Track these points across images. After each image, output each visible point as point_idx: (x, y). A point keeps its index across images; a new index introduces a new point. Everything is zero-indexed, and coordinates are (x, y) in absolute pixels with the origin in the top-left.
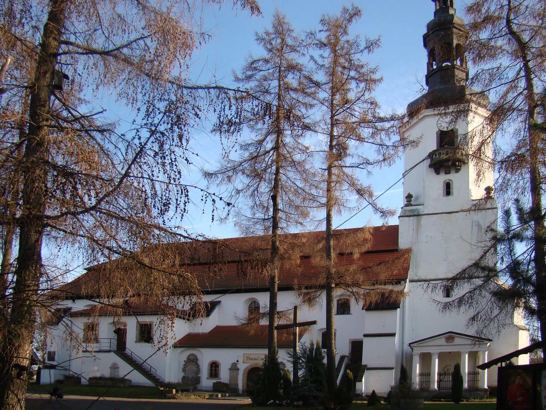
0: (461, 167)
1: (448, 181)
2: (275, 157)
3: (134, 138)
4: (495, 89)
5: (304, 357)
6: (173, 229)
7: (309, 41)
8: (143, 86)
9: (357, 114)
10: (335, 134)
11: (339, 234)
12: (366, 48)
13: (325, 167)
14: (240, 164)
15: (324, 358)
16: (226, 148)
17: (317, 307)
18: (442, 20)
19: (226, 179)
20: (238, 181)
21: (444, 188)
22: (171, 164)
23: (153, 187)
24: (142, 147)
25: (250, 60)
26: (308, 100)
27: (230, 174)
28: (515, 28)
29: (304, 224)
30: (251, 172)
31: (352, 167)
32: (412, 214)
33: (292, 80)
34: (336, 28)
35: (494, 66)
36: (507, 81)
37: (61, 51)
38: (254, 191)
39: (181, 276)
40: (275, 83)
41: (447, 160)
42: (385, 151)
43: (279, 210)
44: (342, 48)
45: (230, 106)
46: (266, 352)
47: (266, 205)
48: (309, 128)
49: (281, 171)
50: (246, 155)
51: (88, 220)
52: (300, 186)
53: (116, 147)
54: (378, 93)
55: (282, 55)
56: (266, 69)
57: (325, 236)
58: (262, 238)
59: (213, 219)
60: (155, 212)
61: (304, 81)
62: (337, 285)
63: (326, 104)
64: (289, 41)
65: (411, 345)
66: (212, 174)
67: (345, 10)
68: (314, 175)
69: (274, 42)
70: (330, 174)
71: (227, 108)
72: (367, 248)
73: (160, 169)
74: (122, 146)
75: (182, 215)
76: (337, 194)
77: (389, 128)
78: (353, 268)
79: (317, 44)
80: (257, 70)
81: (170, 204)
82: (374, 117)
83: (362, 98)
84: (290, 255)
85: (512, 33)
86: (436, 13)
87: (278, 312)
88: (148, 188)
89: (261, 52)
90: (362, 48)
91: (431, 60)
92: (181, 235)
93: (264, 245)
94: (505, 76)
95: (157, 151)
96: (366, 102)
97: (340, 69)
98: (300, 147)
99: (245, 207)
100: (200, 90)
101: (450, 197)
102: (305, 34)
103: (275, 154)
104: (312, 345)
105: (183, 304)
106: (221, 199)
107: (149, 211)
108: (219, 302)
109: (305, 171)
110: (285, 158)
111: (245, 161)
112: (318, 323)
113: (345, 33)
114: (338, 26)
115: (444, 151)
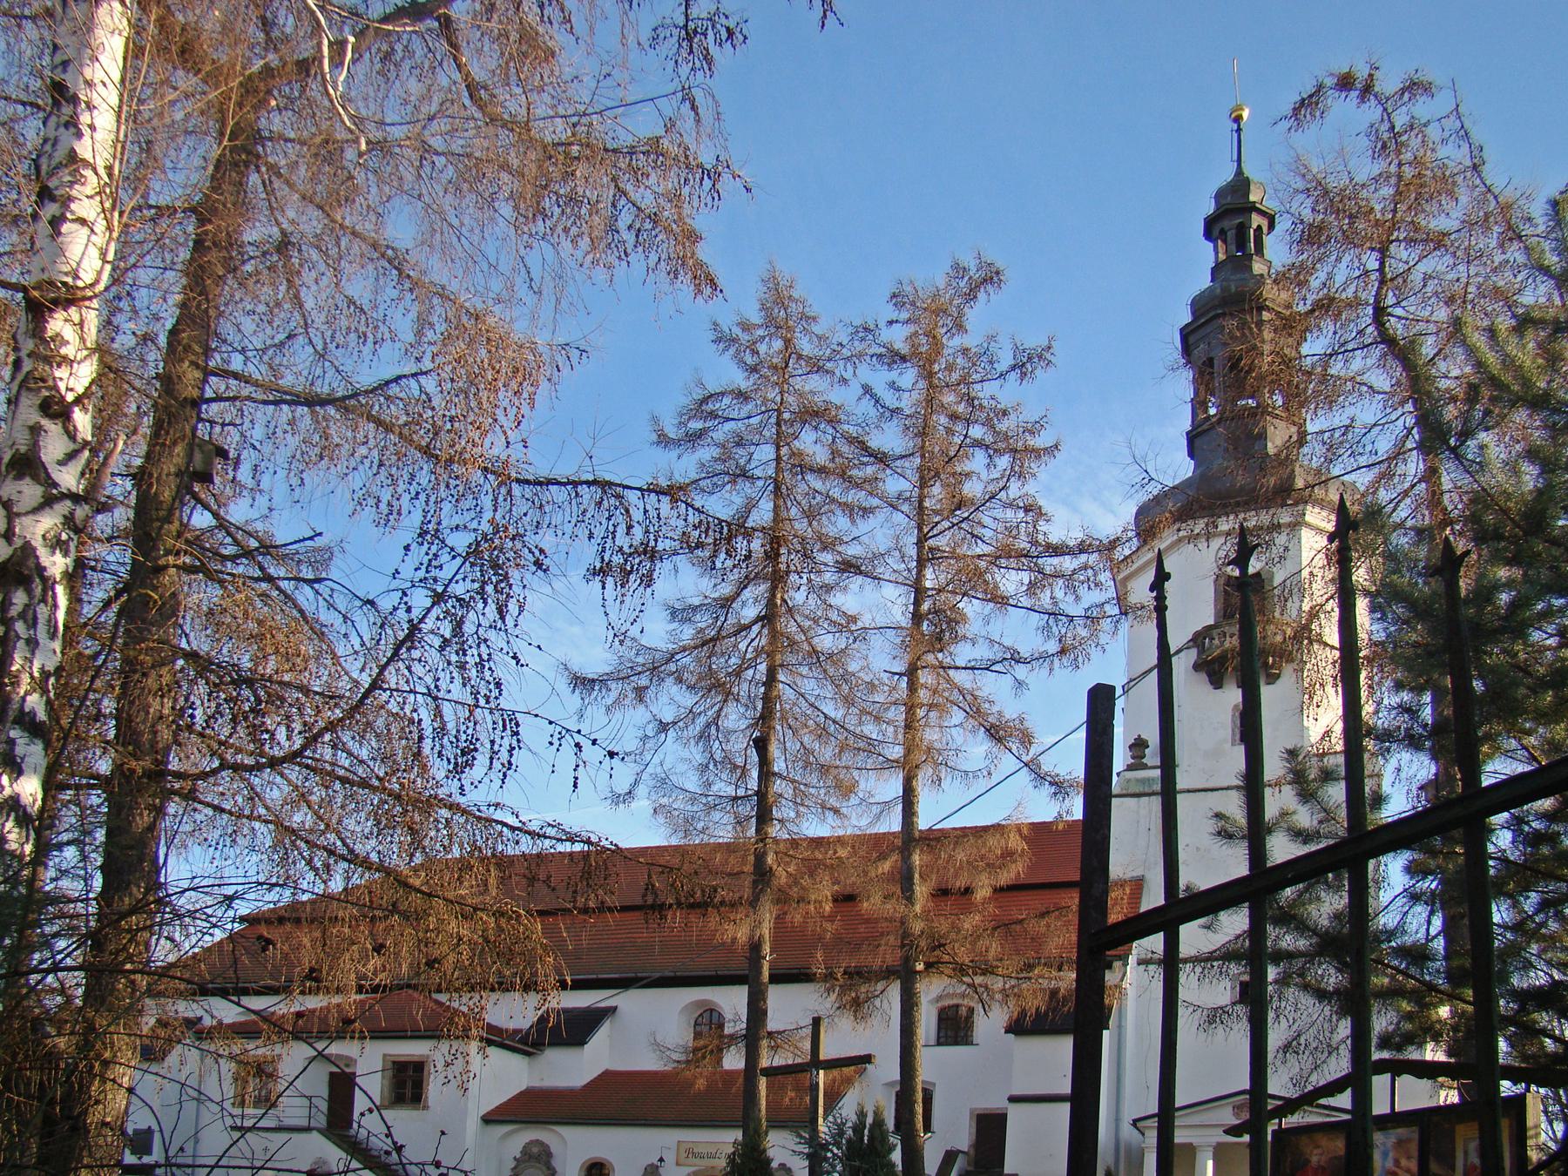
2: (764, 641)
3: (395, 609)
5: (838, 1144)
6: (484, 808)
7: (859, 346)
8: (413, 477)
9: (988, 533)
10: (928, 584)
11: (934, 838)
12: (1013, 368)
13: (900, 667)
14: (671, 657)
15: (892, 1148)
16: (616, 624)
17: (875, 1021)
18: (1233, 289)
19: (631, 695)
20: (664, 699)
22: (480, 665)
23: (438, 713)
24: (414, 628)
25: (698, 394)
26: (855, 496)
27: (644, 681)
28: (1396, 327)
29: (844, 810)
30: (700, 679)
31: (973, 668)
32: (1147, 790)
33: (812, 444)
34: (935, 315)
35: (1337, 422)
36: (1374, 459)
37: (209, 393)
38: (708, 726)
39: (502, 914)
40: (767, 452)
43: (775, 774)
44: (950, 368)
45: (630, 527)
46: (738, 1135)
47: (740, 761)
48: (858, 568)
49: (781, 677)
50: (687, 634)
51: (275, 789)
52: (832, 715)
53: (345, 617)
54: (1041, 484)
55: (785, 381)
56: (743, 415)
57: (898, 842)
58: (729, 848)
59: (575, 786)
60: (439, 769)
61: (845, 448)
62: (929, 965)
63: (905, 508)
64: (805, 346)
65: (1139, 1124)
66: (593, 681)
67: (959, 270)
68: (872, 687)
69: (762, 348)
70: (912, 687)
71: (621, 530)
72: (1013, 875)
73: (455, 674)
74: (364, 622)
75: (505, 775)
76: (931, 735)
77: (1074, 572)
78: (970, 922)
79: (880, 356)
80: (716, 417)
81: (476, 750)
82: (1035, 543)
84: (803, 888)
85: (1387, 340)
86: (1215, 271)
87: (770, 1034)
88: (425, 715)
89: (727, 373)
90: (1003, 366)
92: (505, 824)
93: (733, 863)
94: (1369, 448)
95: (448, 636)
96: (1011, 505)
97: (943, 420)
98: (834, 616)
99: (682, 767)
100: (553, 488)
102: (850, 330)
103: (765, 631)
104: (862, 1115)
105: (515, 1011)
106: (594, 742)
107: (424, 768)
108: (614, 1009)
109: (846, 677)
110: (793, 643)
111: (684, 649)
112: (877, 1061)
113: (960, 327)
114: (940, 311)
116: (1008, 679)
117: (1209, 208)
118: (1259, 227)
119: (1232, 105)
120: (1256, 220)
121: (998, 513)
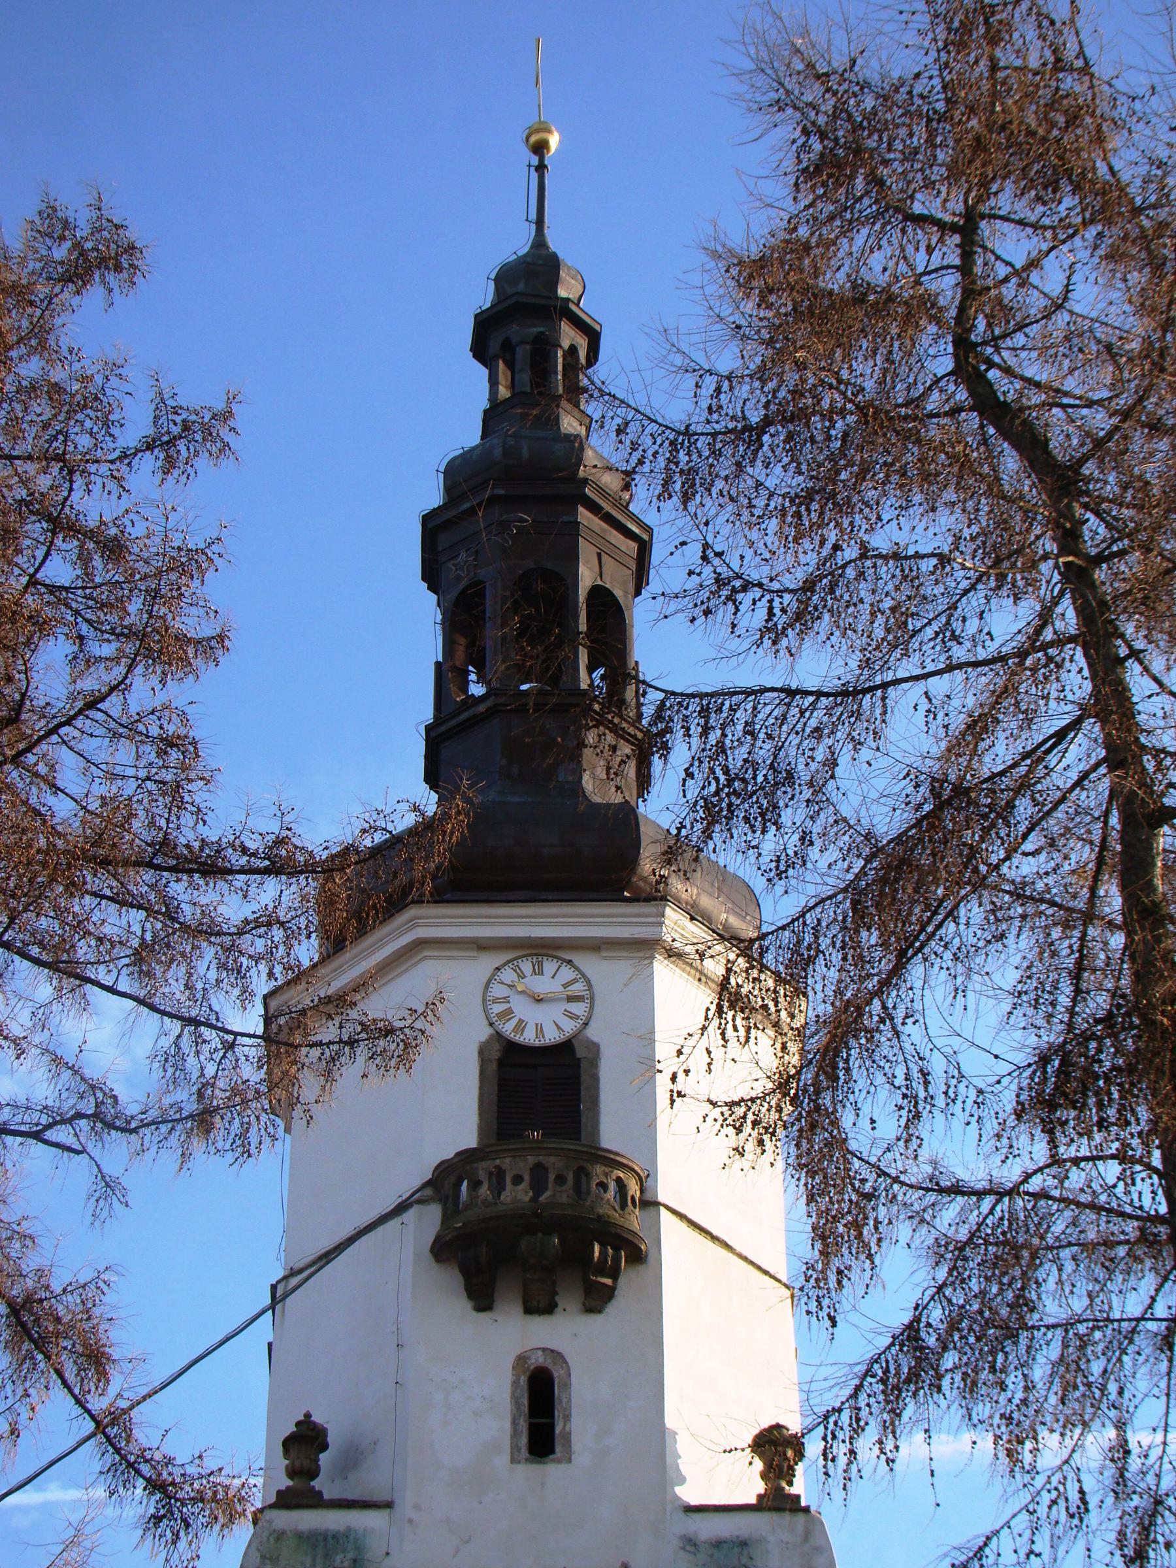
0: (615, 1274)
1: (539, 1359)
4: (920, 687)
21: (515, 1399)
41: (534, 1221)
42: (210, 1070)
67: (53, 224)
77: (247, 927)
83: (113, 705)
86: (492, 417)
90: (129, 438)
91: (460, 654)
94: (973, 625)
101: (552, 1471)
115: (524, 1166)
116: (80, 1170)
117: (484, 296)
118: (573, 350)
119: (532, 121)
120: (568, 336)
121: (97, 747)
